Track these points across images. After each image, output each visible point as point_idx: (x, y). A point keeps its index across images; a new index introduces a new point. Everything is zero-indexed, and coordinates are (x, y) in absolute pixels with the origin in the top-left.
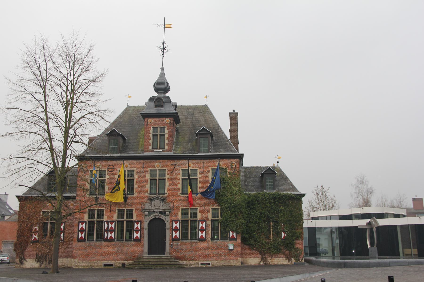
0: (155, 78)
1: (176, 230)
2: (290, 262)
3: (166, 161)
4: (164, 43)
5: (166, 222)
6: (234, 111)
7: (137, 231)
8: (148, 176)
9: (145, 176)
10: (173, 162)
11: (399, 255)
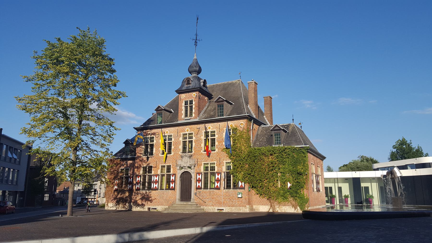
2: (296, 210)
5: (192, 174)
8: (181, 139)
9: (179, 139)
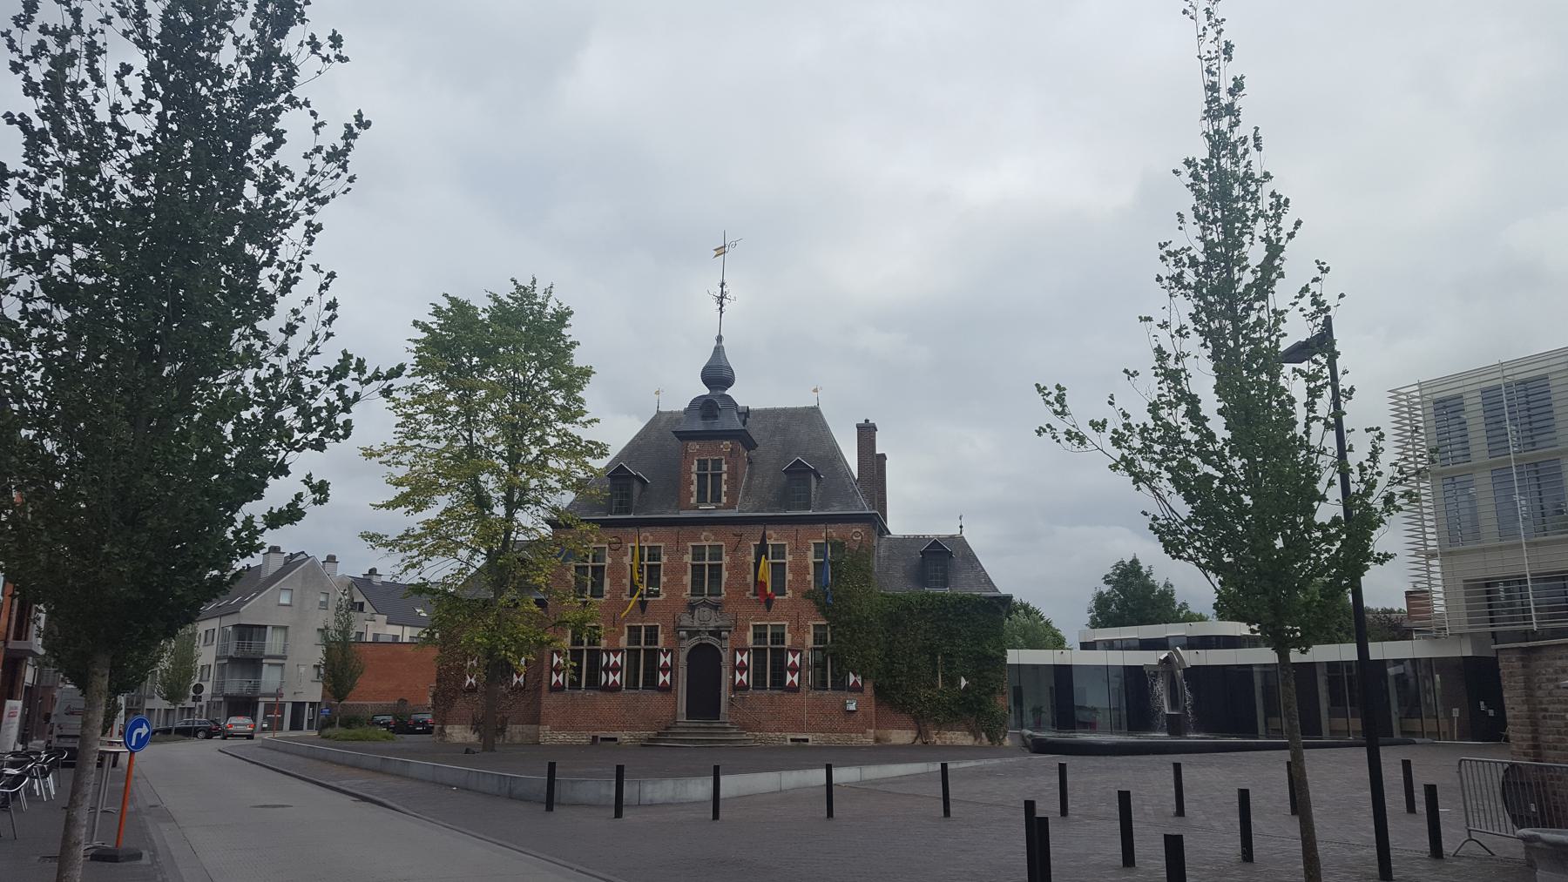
0: (704, 358)
1: (742, 668)
3: (722, 528)
4: (723, 285)
6: (331, 559)
7: (665, 669)
8: (688, 558)
10: (737, 529)
11: (1319, 733)
